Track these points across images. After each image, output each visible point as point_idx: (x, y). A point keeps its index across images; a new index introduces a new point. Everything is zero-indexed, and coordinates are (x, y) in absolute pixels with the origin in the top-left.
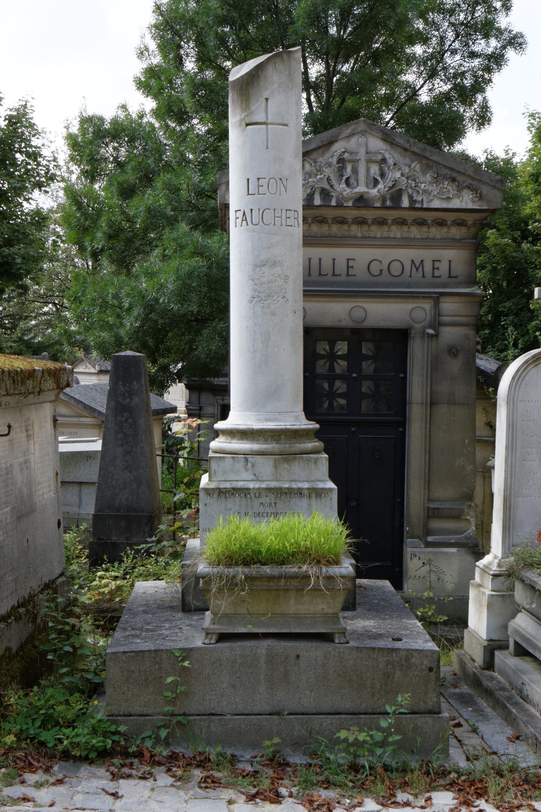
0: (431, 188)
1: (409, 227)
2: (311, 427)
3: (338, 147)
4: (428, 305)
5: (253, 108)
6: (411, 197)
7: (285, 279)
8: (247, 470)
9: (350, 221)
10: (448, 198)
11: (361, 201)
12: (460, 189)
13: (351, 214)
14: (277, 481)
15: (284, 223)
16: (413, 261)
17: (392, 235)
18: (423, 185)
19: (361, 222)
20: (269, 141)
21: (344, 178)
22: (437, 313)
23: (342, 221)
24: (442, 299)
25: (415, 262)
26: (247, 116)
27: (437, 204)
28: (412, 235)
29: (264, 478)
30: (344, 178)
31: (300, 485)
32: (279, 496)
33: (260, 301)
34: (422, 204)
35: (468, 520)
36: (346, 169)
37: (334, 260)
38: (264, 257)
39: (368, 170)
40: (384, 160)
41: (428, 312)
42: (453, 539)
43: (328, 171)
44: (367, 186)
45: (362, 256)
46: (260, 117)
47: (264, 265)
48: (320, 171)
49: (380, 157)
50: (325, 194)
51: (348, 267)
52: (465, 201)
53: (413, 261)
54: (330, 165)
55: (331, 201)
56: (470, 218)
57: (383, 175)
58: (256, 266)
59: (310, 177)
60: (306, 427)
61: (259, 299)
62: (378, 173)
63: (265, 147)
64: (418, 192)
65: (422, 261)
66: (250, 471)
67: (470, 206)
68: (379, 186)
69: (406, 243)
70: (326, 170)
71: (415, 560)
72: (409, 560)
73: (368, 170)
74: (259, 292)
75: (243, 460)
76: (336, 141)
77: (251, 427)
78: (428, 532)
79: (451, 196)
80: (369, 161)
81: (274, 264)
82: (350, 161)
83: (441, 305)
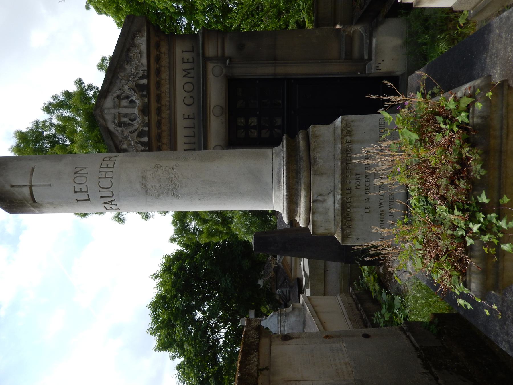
0: (134, 65)
1: (162, 79)
2: (285, 142)
3: (112, 127)
4: (211, 65)
5: (20, 197)
6: (141, 78)
7: (157, 167)
8: (324, 201)
9: (159, 118)
10: (140, 53)
11: (145, 110)
12: (134, 45)
13: (154, 117)
14: (334, 173)
15: (111, 170)
16: (184, 76)
17: (167, 91)
18: (133, 70)
19: (159, 111)
20: (44, 184)
21: (130, 122)
22: (215, 59)
23: (159, 124)
24: (207, 55)
25: (184, 75)
26: (27, 201)
27: (144, 61)
28: (167, 78)
29: (332, 184)
30: (130, 122)
31: (339, 151)
32: (349, 171)
33: (176, 189)
34: (145, 70)
35: (353, 32)
36: (125, 121)
37: (184, 128)
38: (138, 186)
39: (125, 107)
40: (118, 97)
41: (216, 65)
42: (366, 41)
43: (126, 133)
44: (134, 107)
45: (182, 110)
46: (26, 191)
47: (145, 186)
48: (126, 138)
49: (116, 99)
50: (141, 134)
51: (189, 118)
52: (142, 42)
53: (184, 76)
54: (122, 132)
55: (145, 131)
56: (154, 40)
57: (127, 97)
58: (147, 193)
59: (131, 144)
60: (285, 146)
61: (174, 190)
62: (126, 101)
63: (49, 187)
64: (137, 73)
65: (184, 70)
66: (326, 198)
67: (145, 38)
68: (134, 99)
69: (172, 81)
70: (125, 134)
71: (381, 67)
72: (380, 71)
73: (125, 107)
74: (169, 190)
75: (315, 204)
76: (108, 128)
77: (285, 196)
78: (361, 58)
79: (138, 51)
80: (119, 106)
81: (144, 177)
82: (120, 119)
83: (211, 56)
